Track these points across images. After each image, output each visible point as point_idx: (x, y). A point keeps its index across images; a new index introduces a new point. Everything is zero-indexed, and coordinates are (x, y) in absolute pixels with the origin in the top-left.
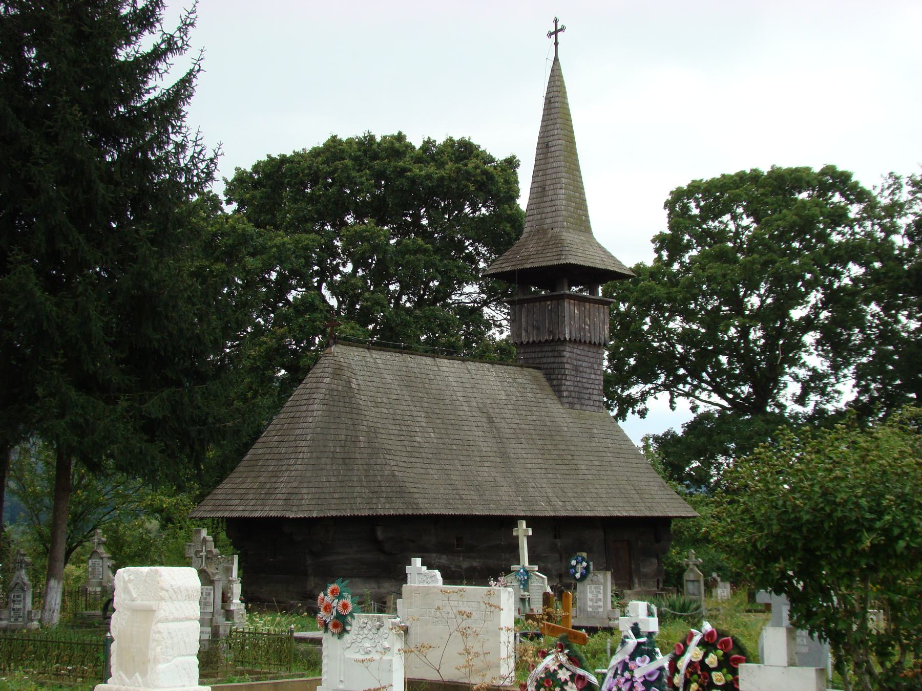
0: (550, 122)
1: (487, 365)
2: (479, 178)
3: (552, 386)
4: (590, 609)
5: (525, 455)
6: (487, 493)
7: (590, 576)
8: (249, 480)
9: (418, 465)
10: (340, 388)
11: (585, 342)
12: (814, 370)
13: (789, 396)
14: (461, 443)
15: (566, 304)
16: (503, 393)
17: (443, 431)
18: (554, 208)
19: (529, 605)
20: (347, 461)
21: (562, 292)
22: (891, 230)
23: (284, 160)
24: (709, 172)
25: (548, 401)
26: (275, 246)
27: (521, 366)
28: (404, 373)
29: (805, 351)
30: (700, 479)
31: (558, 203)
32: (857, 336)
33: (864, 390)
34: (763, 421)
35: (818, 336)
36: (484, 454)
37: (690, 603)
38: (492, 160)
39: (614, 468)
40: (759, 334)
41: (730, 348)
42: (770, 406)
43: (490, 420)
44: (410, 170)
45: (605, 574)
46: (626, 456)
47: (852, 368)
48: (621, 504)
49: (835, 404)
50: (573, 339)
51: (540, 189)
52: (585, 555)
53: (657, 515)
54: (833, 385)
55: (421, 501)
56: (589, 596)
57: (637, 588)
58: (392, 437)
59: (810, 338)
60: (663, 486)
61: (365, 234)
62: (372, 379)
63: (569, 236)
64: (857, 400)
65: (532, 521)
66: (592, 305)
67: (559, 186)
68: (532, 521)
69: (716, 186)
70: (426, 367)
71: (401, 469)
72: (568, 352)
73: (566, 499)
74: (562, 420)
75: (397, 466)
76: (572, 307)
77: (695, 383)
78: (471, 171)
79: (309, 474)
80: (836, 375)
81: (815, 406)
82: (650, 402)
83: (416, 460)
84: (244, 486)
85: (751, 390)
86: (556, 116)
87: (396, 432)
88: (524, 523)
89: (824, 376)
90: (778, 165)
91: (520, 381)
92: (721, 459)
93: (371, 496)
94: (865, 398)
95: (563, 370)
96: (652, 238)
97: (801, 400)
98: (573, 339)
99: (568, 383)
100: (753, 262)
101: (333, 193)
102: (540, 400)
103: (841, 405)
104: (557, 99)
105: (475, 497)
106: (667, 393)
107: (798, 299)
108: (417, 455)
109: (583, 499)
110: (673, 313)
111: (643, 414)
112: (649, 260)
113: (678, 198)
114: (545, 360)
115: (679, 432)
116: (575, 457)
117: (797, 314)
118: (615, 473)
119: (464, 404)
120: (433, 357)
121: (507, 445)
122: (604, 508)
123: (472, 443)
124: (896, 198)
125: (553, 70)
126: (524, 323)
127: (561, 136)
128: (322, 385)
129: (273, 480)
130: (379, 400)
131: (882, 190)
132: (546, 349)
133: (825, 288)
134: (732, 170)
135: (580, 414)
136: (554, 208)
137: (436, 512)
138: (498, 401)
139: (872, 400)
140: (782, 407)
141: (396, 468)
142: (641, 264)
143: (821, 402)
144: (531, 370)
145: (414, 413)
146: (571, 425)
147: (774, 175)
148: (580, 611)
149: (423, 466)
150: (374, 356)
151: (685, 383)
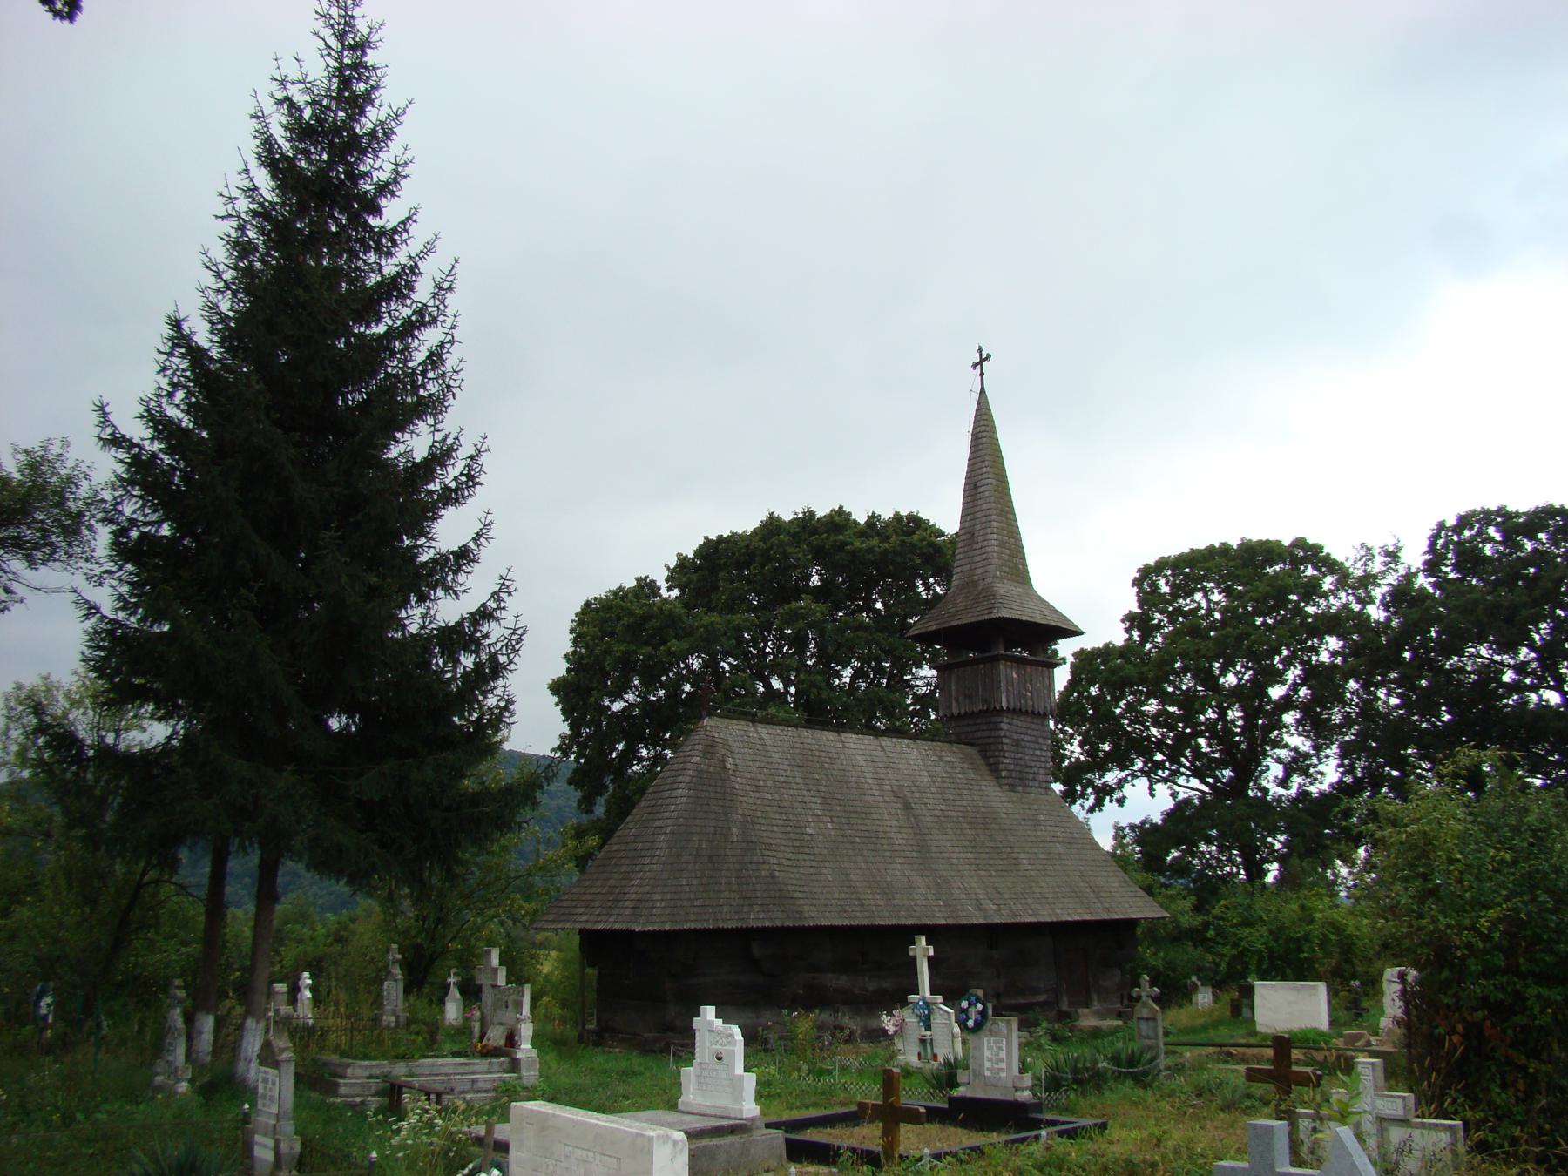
0: (979, 460)
1: (906, 741)
2: (925, 551)
3: (989, 765)
4: (988, 1073)
5: (950, 849)
6: (897, 896)
7: (988, 1025)
8: (599, 883)
9: (808, 863)
10: (711, 769)
11: (1027, 711)
12: (1296, 749)
13: (1271, 778)
14: (867, 834)
15: (1002, 667)
16: (926, 774)
17: (844, 821)
18: (984, 556)
19: (932, 1049)
20: (715, 859)
21: (996, 653)
22: (1367, 600)
23: (720, 539)
24: (1176, 547)
25: (983, 782)
26: (703, 626)
27: (950, 742)
28: (798, 751)
29: (1287, 733)
30: (1181, 869)
31: (989, 549)
32: (1337, 717)
33: (1350, 770)
34: (1245, 805)
35: (1298, 715)
36: (897, 848)
37: (1142, 1053)
38: (941, 534)
39: (1063, 862)
40: (1238, 714)
41: (1210, 730)
42: (1252, 790)
43: (907, 806)
44: (851, 544)
45: (1008, 1022)
46: (1080, 846)
47: (1334, 747)
48: (1070, 906)
49: (1318, 785)
50: (1011, 708)
51: (968, 536)
52: (980, 992)
53: (1117, 917)
54: (1316, 766)
55: (806, 908)
56: (987, 1053)
57: (1096, 1006)
58: (776, 829)
59: (1289, 718)
60: (1126, 882)
61: (800, 611)
62: (755, 758)
63: (1004, 588)
64: (1340, 781)
65: (933, 933)
66: (1034, 668)
67: (989, 530)
68: (934, 933)
69: (1184, 561)
70: (828, 744)
71: (782, 868)
72: (1005, 724)
73: (1002, 902)
74: (1000, 805)
75: (779, 864)
76: (1009, 670)
77: (1173, 768)
78: (917, 543)
79: (665, 876)
80: (1317, 755)
81: (1299, 788)
82: (1127, 789)
83: (805, 857)
84: (594, 890)
85: (1232, 774)
86: (984, 452)
87: (781, 822)
88: (923, 939)
89: (1306, 756)
90: (1248, 537)
91: (948, 759)
92: (1203, 847)
93: (742, 902)
94: (1348, 779)
95: (1000, 746)
96: (1121, 617)
97: (1284, 782)
98: (1011, 708)
99: (1007, 761)
100: (1227, 636)
101: (768, 570)
102: (972, 782)
103: (1325, 787)
104: (985, 434)
105: (882, 903)
106: (1146, 779)
107: (1277, 677)
108: (807, 850)
109: (1023, 901)
110: (1149, 696)
111: (1121, 802)
112: (1118, 638)
113: (1145, 577)
114: (979, 734)
115: (1158, 819)
116: (1015, 850)
117: (1276, 692)
118: (1065, 868)
119: (874, 787)
120: (837, 732)
121: (927, 837)
122: (1050, 912)
123: (882, 835)
124: (1369, 569)
125: (979, 404)
126: (954, 693)
127: (990, 475)
128: (689, 765)
129: (624, 883)
130: (762, 783)
131: (1355, 562)
132: (979, 721)
133: (1302, 663)
134: (1201, 544)
135: (1022, 797)
136: (984, 556)
137: (824, 923)
138: (918, 784)
139: (1357, 781)
140: (1265, 791)
141: (776, 867)
142: (1110, 643)
143: (1304, 785)
144: (962, 746)
145: (806, 799)
146: (1010, 810)
147: (1244, 547)
148: (975, 1075)
149: (814, 864)
150: (760, 730)
151: (1164, 769)
